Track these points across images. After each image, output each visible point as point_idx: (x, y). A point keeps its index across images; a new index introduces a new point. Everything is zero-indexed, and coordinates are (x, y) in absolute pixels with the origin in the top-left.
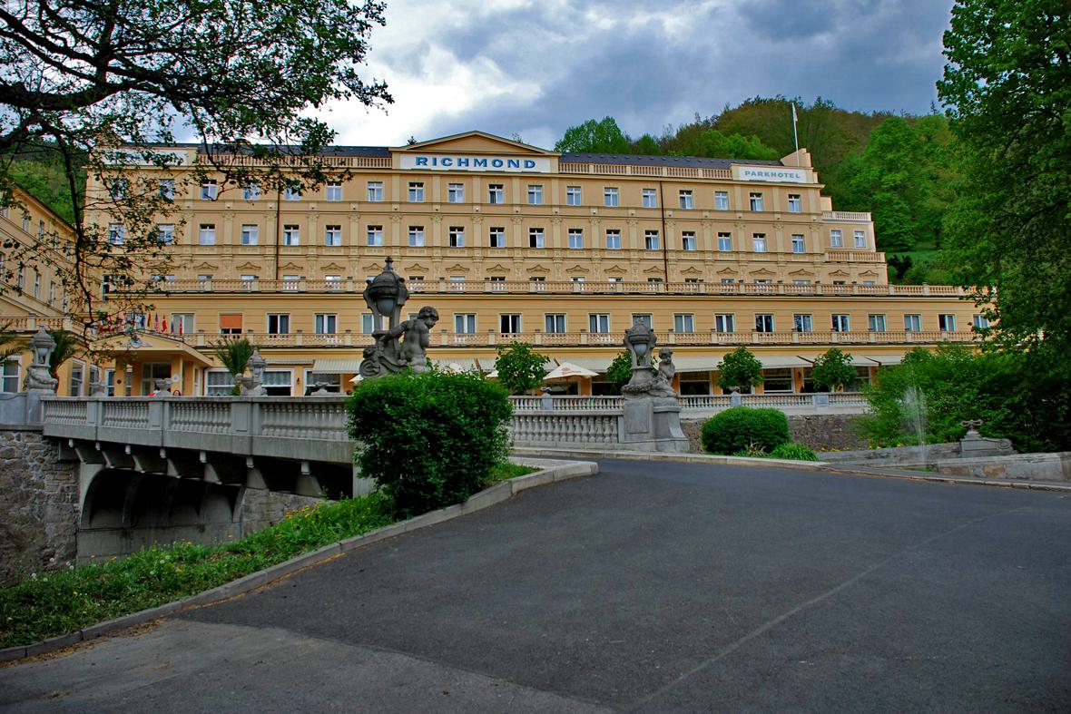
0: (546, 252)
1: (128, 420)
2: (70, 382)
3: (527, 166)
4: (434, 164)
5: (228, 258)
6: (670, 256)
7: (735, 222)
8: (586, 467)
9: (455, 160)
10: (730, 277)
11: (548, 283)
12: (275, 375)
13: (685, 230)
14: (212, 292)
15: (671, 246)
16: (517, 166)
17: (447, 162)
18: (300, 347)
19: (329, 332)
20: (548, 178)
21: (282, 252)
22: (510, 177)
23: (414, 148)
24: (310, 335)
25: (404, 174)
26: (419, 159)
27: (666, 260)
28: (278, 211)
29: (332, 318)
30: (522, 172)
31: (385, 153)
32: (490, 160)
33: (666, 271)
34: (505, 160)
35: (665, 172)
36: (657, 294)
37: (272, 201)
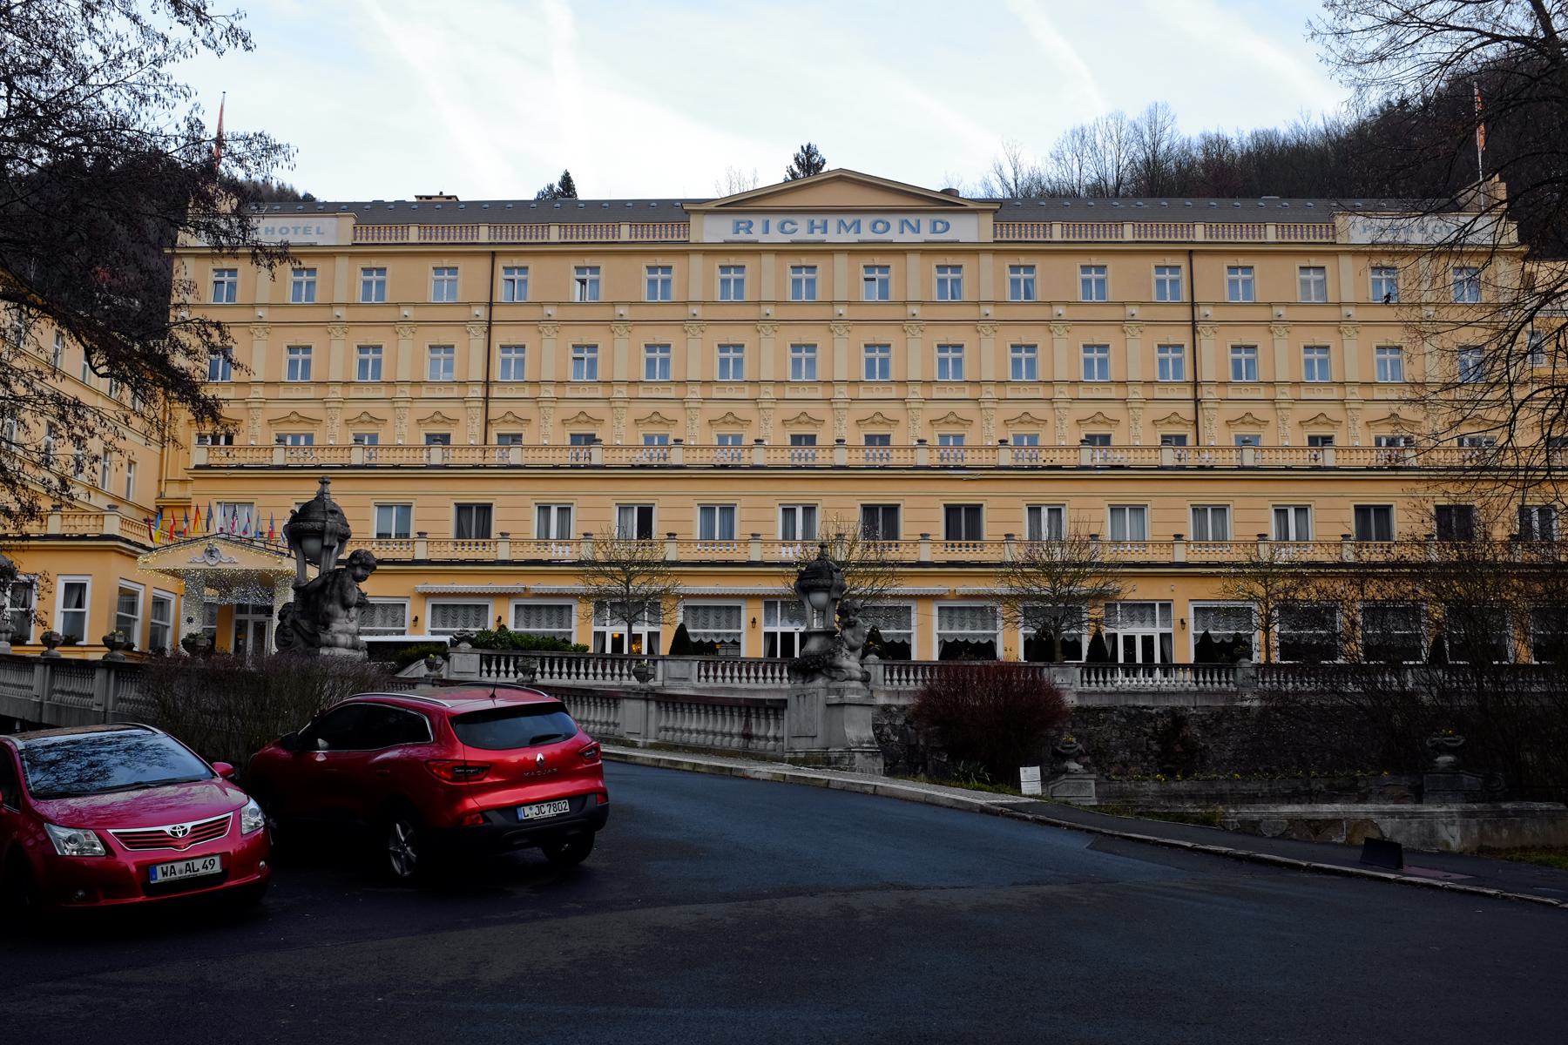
0: (456, 388)
1: (14, 686)
2: (114, 619)
3: (934, 231)
4: (763, 231)
5: (842, 406)
6: (1204, 393)
7: (1337, 324)
8: (564, 807)
9: (802, 222)
10: (735, 430)
11: (527, 448)
12: (461, 612)
13: (1237, 343)
14: (445, 467)
15: (1206, 374)
16: (917, 230)
17: (788, 227)
18: (504, 563)
19: (785, 537)
20: (974, 251)
21: (495, 392)
22: (902, 251)
23: (740, 206)
24: (690, 542)
25: (709, 251)
26: (738, 223)
27: (1197, 401)
28: (490, 321)
29: (564, 511)
30: (926, 242)
31: (676, 212)
32: (866, 221)
33: (1196, 422)
34: (894, 221)
35: (1199, 233)
36: (1240, 468)
37: (478, 304)
